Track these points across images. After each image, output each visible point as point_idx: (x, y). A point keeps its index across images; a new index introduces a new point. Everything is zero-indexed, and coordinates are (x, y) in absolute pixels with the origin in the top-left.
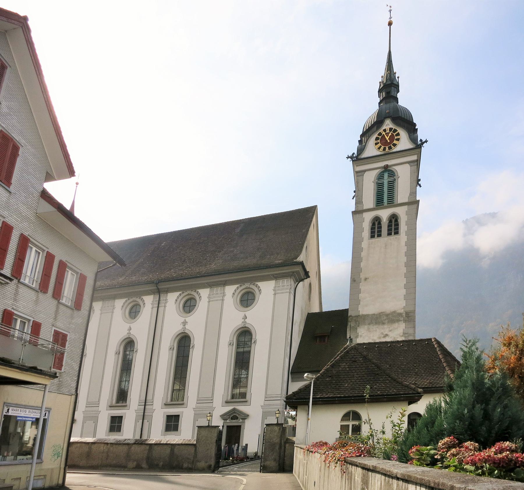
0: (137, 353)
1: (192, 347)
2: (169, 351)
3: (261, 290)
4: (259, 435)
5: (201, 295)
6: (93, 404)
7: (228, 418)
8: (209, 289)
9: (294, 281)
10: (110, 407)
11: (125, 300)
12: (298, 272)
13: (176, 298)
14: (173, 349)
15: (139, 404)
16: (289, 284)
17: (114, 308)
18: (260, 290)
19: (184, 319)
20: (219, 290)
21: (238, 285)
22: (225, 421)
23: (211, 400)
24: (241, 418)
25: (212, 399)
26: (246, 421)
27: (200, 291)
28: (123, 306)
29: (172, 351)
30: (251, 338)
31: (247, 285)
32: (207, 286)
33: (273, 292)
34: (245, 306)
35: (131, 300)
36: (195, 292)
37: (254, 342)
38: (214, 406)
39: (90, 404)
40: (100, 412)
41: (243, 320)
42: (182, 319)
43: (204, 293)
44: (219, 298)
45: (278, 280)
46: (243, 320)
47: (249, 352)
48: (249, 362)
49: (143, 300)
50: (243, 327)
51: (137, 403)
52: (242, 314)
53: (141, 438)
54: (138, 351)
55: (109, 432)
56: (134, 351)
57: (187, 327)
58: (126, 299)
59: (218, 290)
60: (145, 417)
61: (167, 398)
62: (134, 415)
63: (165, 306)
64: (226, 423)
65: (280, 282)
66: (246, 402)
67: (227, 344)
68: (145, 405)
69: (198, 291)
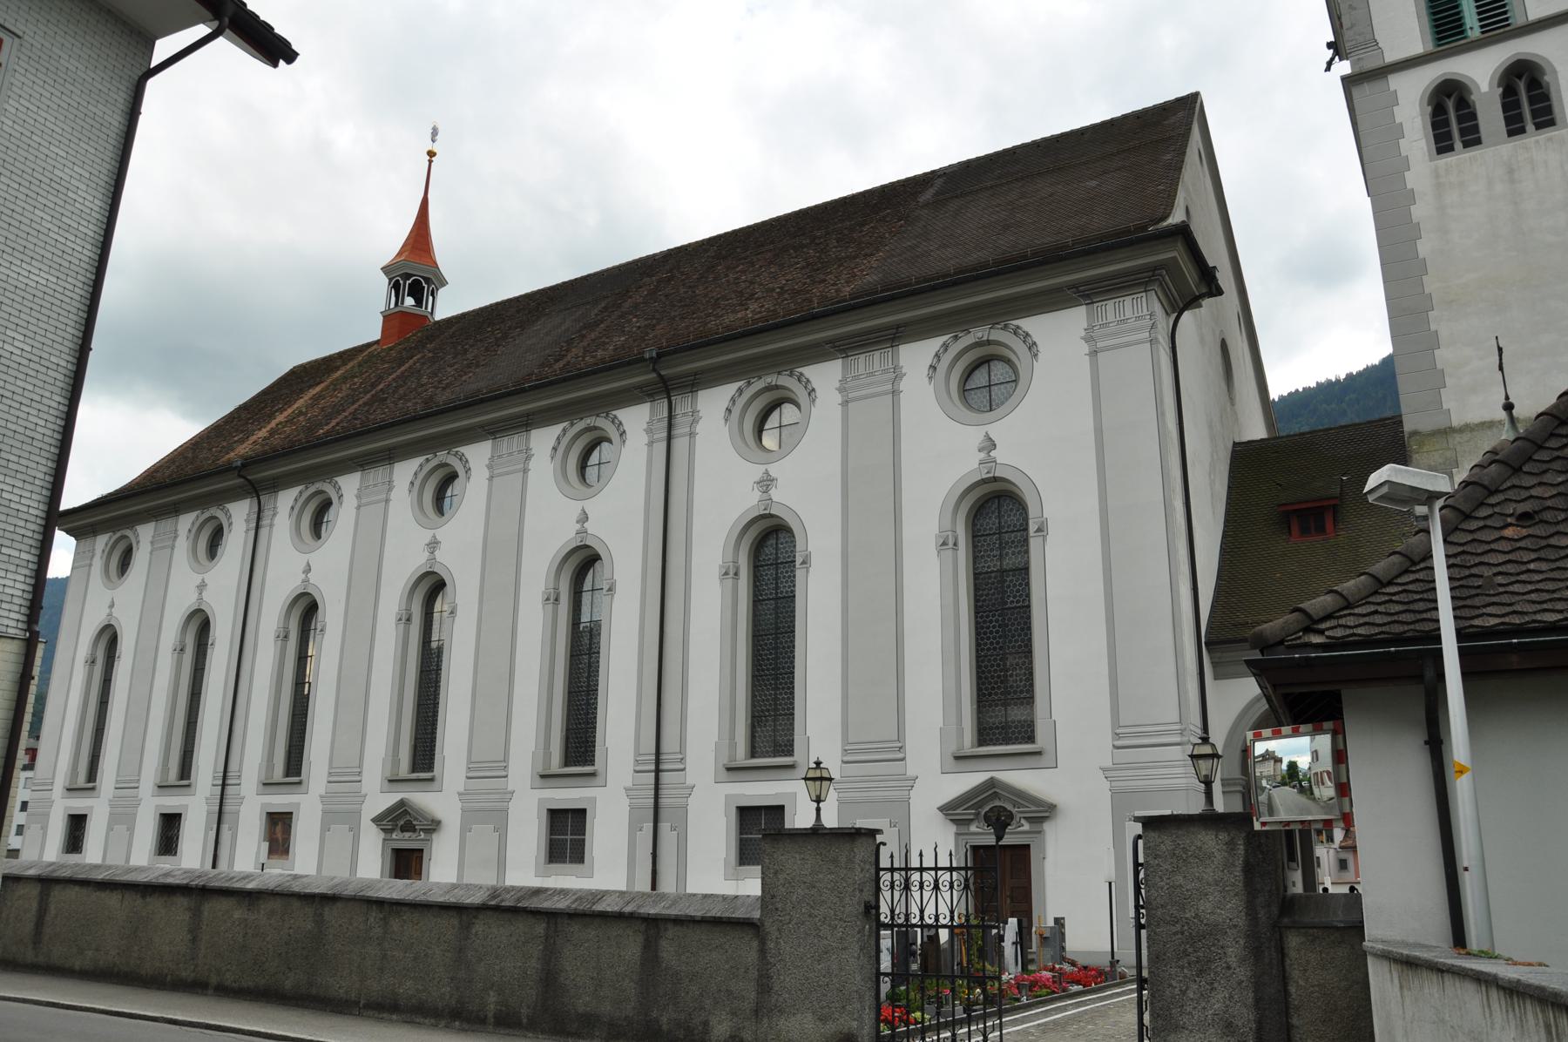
0: (612, 595)
1: (804, 562)
2: (721, 580)
3: (1035, 343)
4: (1110, 884)
5: (815, 384)
6: (491, 769)
7: (972, 817)
8: (840, 361)
9: (1161, 303)
10: (543, 777)
11: (562, 428)
12: (1171, 267)
13: (725, 404)
14: (736, 574)
15: (117, 786)
16: (890, 364)
17: (528, 458)
18: (1032, 347)
19: (981, 437)
20: (515, 445)
21: (945, 338)
22: (963, 829)
23: (896, 750)
24: (1024, 818)
25: (901, 748)
26: (1047, 826)
27: (810, 371)
28: (555, 449)
29: (950, 552)
30: (1026, 520)
31: (979, 333)
32: (832, 350)
33: (1085, 348)
34: (985, 406)
35: (759, 385)
36: (791, 375)
37: (1039, 530)
38: (510, 789)
39: (338, 774)
40: (365, 796)
41: (982, 455)
42: (427, 536)
43: (478, 454)
44: (380, 497)
45: (1100, 304)
46: (982, 455)
47: (1025, 570)
48: (1029, 606)
49: (616, 421)
50: (984, 481)
51: (630, 767)
52: (975, 435)
53: (654, 887)
54: (814, 560)
55: (545, 864)
56: (798, 563)
57: (776, 495)
58: (945, 338)
59: (872, 362)
60: (663, 814)
61: (960, 731)
62: (624, 804)
63: (692, 435)
64: (966, 834)
65: (1111, 310)
66: (1039, 753)
67: (539, 599)
68: (658, 771)
69: (801, 374)
